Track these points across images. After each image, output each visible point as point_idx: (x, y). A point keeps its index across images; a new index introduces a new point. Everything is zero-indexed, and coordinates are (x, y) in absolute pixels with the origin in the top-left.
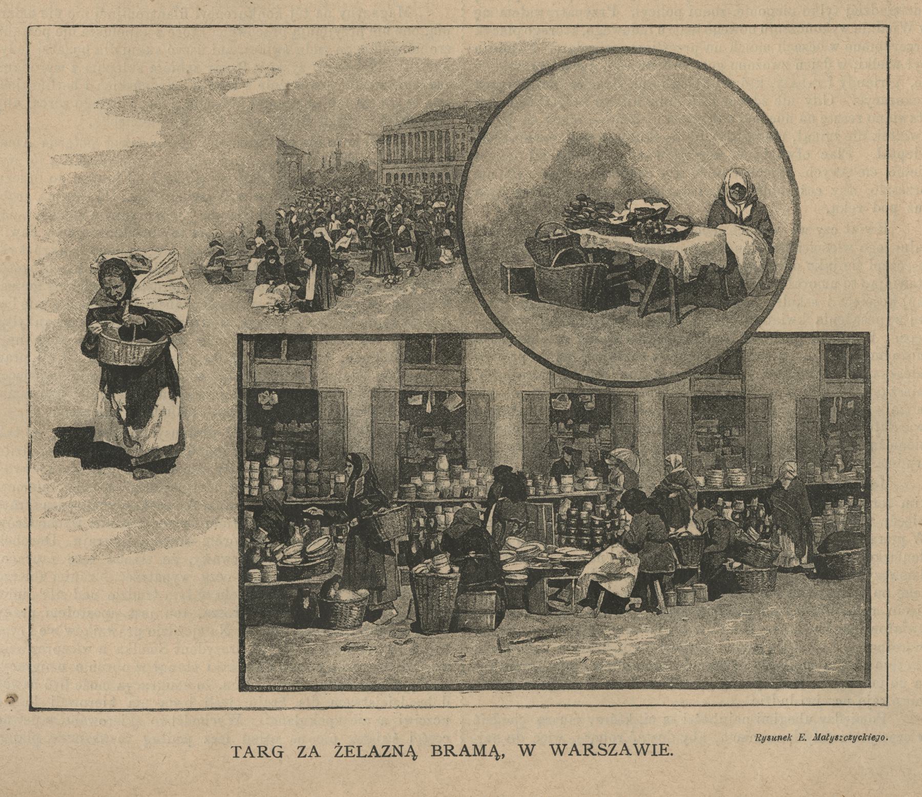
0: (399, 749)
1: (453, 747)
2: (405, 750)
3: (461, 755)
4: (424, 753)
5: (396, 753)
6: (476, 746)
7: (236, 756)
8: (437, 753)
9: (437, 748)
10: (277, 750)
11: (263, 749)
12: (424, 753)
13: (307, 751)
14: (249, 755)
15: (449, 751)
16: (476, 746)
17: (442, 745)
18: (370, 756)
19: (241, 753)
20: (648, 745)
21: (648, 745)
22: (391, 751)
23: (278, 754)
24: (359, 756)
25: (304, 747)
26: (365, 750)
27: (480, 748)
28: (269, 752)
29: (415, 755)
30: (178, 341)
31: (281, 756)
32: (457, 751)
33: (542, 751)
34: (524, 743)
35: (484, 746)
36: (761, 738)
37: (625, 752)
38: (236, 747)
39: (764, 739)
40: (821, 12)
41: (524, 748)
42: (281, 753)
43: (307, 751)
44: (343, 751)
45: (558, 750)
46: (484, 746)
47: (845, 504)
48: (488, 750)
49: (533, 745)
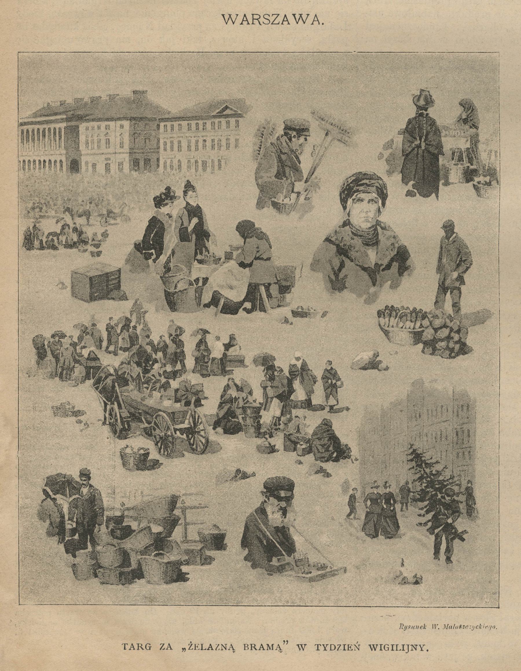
0: (225, 646)
1: (255, 645)
2: (228, 647)
3: (208, 649)
4: (239, 648)
5: (223, 648)
6: (268, 645)
7: (318, 650)
8: (246, 648)
9: (246, 645)
10: (148, 645)
11: (253, 646)
12: (239, 648)
13: (166, 646)
14: (262, 649)
15: (253, 647)
16: (268, 645)
17: (249, 644)
18: (208, 649)
19: (128, 647)
20: (377, 645)
21: (377, 645)
22: (220, 647)
23: (148, 648)
24: (202, 649)
25: (164, 644)
26: (206, 646)
27: (270, 645)
28: (144, 647)
29: (233, 649)
30: (140, 538)
31: (150, 649)
32: (258, 647)
33: (311, 648)
34: (372, 644)
35: (272, 645)
36: (403, 627)
37: (169, 648)
38: (125, 644)
39: (406, 628)
40: (391, 457)
41: (372, 646)
42: (150, 647)
43: (166, 646)
44: (193, 647)
45: (373, 647)
46: (272, 645)
47: (432, 471)
48: (275, 647)
49: (305, 645)
